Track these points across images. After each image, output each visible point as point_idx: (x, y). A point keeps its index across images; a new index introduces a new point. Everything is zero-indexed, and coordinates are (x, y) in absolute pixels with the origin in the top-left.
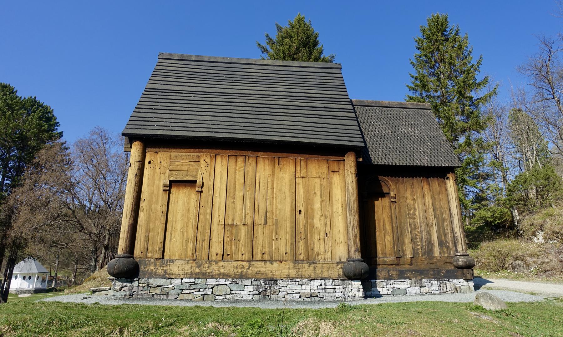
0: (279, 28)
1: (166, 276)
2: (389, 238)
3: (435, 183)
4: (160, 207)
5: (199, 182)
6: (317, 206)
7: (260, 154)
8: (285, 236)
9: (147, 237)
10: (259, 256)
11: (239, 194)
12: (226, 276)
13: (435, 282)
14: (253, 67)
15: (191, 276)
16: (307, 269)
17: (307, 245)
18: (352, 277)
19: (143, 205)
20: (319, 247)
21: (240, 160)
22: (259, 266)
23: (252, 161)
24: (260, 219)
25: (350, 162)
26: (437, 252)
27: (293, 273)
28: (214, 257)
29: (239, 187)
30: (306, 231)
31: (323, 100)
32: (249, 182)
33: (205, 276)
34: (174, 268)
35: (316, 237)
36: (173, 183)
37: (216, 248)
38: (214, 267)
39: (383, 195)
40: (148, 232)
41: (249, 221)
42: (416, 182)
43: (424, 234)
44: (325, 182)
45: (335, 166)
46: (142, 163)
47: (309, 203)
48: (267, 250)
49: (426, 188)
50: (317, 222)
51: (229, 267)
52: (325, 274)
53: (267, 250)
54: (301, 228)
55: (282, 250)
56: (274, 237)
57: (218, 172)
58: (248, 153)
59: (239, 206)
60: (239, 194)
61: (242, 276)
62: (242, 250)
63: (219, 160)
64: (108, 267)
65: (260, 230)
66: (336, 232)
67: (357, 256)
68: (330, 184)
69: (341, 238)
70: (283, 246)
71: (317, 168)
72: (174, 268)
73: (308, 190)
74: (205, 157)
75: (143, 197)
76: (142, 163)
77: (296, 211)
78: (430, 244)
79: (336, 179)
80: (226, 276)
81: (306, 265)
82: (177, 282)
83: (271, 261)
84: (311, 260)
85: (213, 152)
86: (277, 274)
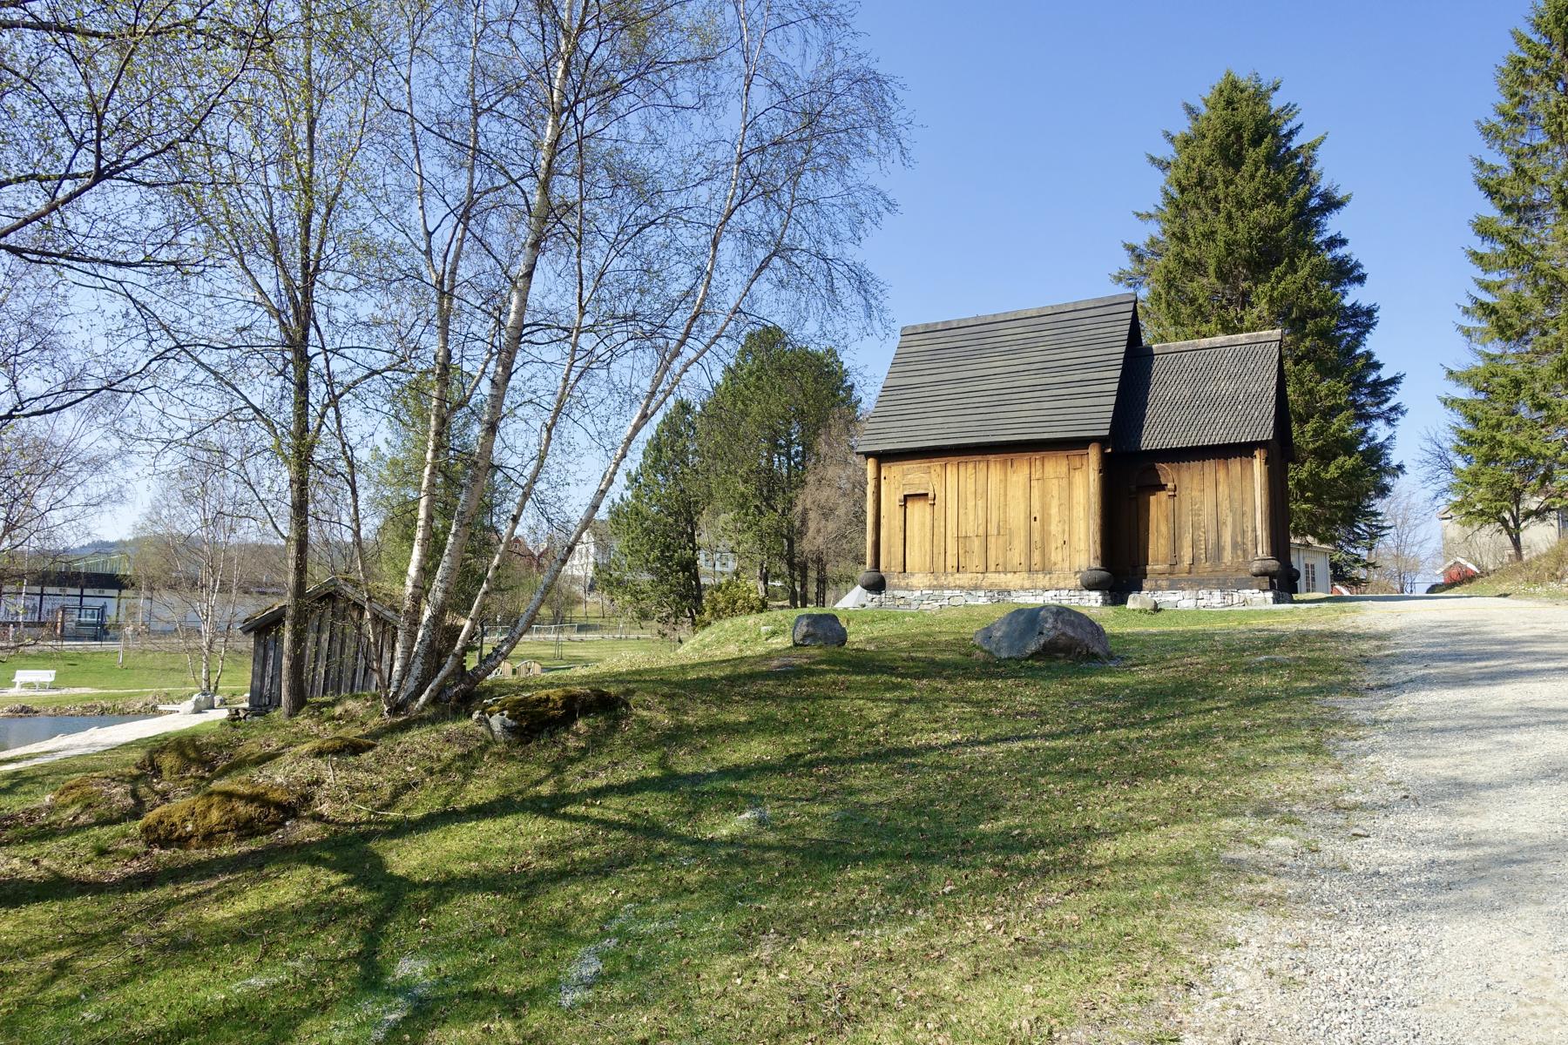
0: (1190, 110)
1: (908, 588)
2: (1162, 541)
3: (1235, 465)
4: (899, 522)
5: (931, 495)
6: (1054, 511)
7: (991, 457)
8: (1019, 545)
9: (889, 552)
10: (992, 567)
11: (971, 504)
12: (961, 588)
13: (1217, 593)
14: (1012, 324)
15: (929, 588)
16: (1041, 580)
17: (1043, 554)
18: (1090, 587)
19: (883, 521)
20: (1055, 556)
21: (971, 466)
22: (992, 578)
23: (983, 466)
24: (993, 530)
25: (1093, 453)
26: (1227, 556)
27: (1027, 584)
28: (949, 570)
29: (971, 497)
30: (1043, 539)
31: (1086, 367)
32: (980, 491)
33: (942, 587)
34: (915, 581)
35: (1053, 546)
36: (906, 497)
37: (952, 561)
38: (950, 579)
39: (1163, 487)
40: (890, 547)
41: (981, 531)
42: (1196, 465)
43: (1212, 537)
44: (1064, 483)
45: (1077, 462)
46: (878, 479)
47: (1045, 507)
48: (1001, 561)
49: (1222, 474)
50: (1055, 528)
51: (964, 579)
52: (1061, 585)
53: (1001, 561)
54: (1036, 537)
55: (1016, 561)
56: (1008, 547)
57: (951, 482)
58: (979, 458)
59: (971, 517)
60: (971, 504)
61: (976, 588)
62: (976, 561)
63: (949, 468)
64: (461, 524)
65: (992, 540)
66: (1075, 538)
67: (1096, 565)
68: (1070, 483)
69: (1082, 546)
70: (1017, 556)
71: (1054, 467)
72: (915, 581)
73: (1044, 494)
74: (936, 465)
75: (883, 513)
76: (878, 479)
77: (1031, 518)
78: (1219, 548)
79: (1078, 478)
80: (961, 588)
81: (1041, 576)
82: (917, 593)
83: (1005, 572)
84: (1046, 570)
85: (942, 461)
86: (1011, 586)
